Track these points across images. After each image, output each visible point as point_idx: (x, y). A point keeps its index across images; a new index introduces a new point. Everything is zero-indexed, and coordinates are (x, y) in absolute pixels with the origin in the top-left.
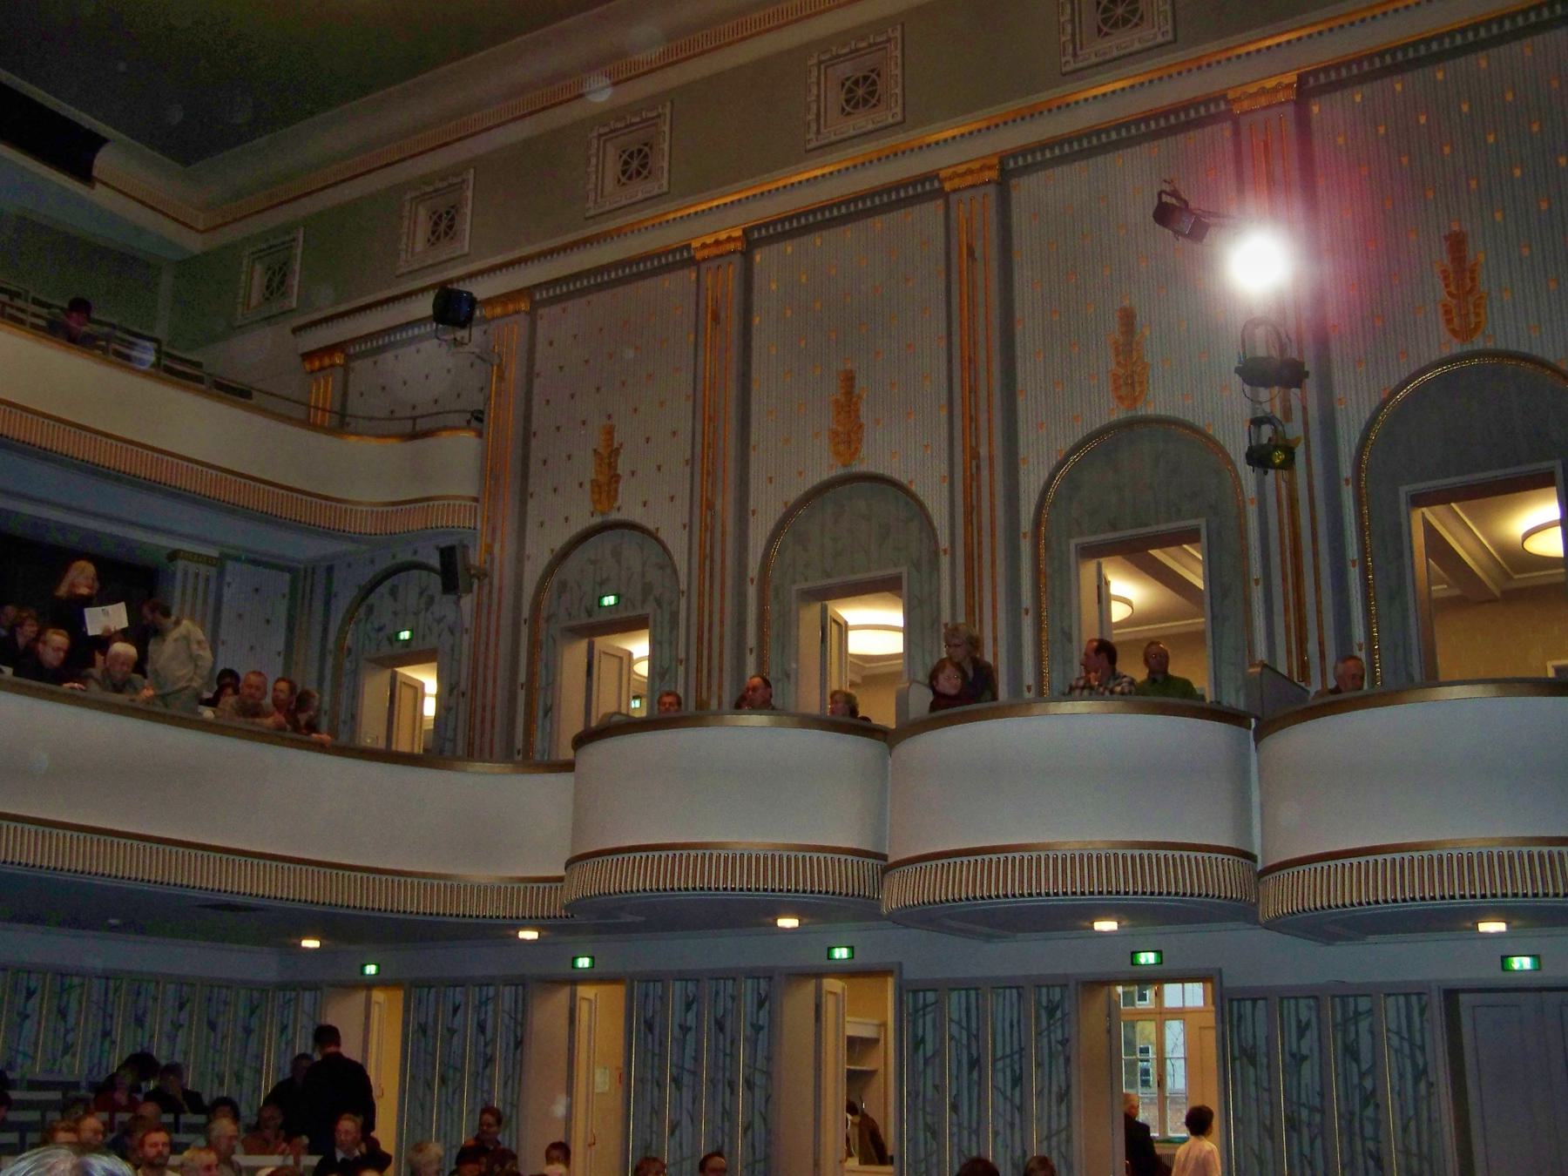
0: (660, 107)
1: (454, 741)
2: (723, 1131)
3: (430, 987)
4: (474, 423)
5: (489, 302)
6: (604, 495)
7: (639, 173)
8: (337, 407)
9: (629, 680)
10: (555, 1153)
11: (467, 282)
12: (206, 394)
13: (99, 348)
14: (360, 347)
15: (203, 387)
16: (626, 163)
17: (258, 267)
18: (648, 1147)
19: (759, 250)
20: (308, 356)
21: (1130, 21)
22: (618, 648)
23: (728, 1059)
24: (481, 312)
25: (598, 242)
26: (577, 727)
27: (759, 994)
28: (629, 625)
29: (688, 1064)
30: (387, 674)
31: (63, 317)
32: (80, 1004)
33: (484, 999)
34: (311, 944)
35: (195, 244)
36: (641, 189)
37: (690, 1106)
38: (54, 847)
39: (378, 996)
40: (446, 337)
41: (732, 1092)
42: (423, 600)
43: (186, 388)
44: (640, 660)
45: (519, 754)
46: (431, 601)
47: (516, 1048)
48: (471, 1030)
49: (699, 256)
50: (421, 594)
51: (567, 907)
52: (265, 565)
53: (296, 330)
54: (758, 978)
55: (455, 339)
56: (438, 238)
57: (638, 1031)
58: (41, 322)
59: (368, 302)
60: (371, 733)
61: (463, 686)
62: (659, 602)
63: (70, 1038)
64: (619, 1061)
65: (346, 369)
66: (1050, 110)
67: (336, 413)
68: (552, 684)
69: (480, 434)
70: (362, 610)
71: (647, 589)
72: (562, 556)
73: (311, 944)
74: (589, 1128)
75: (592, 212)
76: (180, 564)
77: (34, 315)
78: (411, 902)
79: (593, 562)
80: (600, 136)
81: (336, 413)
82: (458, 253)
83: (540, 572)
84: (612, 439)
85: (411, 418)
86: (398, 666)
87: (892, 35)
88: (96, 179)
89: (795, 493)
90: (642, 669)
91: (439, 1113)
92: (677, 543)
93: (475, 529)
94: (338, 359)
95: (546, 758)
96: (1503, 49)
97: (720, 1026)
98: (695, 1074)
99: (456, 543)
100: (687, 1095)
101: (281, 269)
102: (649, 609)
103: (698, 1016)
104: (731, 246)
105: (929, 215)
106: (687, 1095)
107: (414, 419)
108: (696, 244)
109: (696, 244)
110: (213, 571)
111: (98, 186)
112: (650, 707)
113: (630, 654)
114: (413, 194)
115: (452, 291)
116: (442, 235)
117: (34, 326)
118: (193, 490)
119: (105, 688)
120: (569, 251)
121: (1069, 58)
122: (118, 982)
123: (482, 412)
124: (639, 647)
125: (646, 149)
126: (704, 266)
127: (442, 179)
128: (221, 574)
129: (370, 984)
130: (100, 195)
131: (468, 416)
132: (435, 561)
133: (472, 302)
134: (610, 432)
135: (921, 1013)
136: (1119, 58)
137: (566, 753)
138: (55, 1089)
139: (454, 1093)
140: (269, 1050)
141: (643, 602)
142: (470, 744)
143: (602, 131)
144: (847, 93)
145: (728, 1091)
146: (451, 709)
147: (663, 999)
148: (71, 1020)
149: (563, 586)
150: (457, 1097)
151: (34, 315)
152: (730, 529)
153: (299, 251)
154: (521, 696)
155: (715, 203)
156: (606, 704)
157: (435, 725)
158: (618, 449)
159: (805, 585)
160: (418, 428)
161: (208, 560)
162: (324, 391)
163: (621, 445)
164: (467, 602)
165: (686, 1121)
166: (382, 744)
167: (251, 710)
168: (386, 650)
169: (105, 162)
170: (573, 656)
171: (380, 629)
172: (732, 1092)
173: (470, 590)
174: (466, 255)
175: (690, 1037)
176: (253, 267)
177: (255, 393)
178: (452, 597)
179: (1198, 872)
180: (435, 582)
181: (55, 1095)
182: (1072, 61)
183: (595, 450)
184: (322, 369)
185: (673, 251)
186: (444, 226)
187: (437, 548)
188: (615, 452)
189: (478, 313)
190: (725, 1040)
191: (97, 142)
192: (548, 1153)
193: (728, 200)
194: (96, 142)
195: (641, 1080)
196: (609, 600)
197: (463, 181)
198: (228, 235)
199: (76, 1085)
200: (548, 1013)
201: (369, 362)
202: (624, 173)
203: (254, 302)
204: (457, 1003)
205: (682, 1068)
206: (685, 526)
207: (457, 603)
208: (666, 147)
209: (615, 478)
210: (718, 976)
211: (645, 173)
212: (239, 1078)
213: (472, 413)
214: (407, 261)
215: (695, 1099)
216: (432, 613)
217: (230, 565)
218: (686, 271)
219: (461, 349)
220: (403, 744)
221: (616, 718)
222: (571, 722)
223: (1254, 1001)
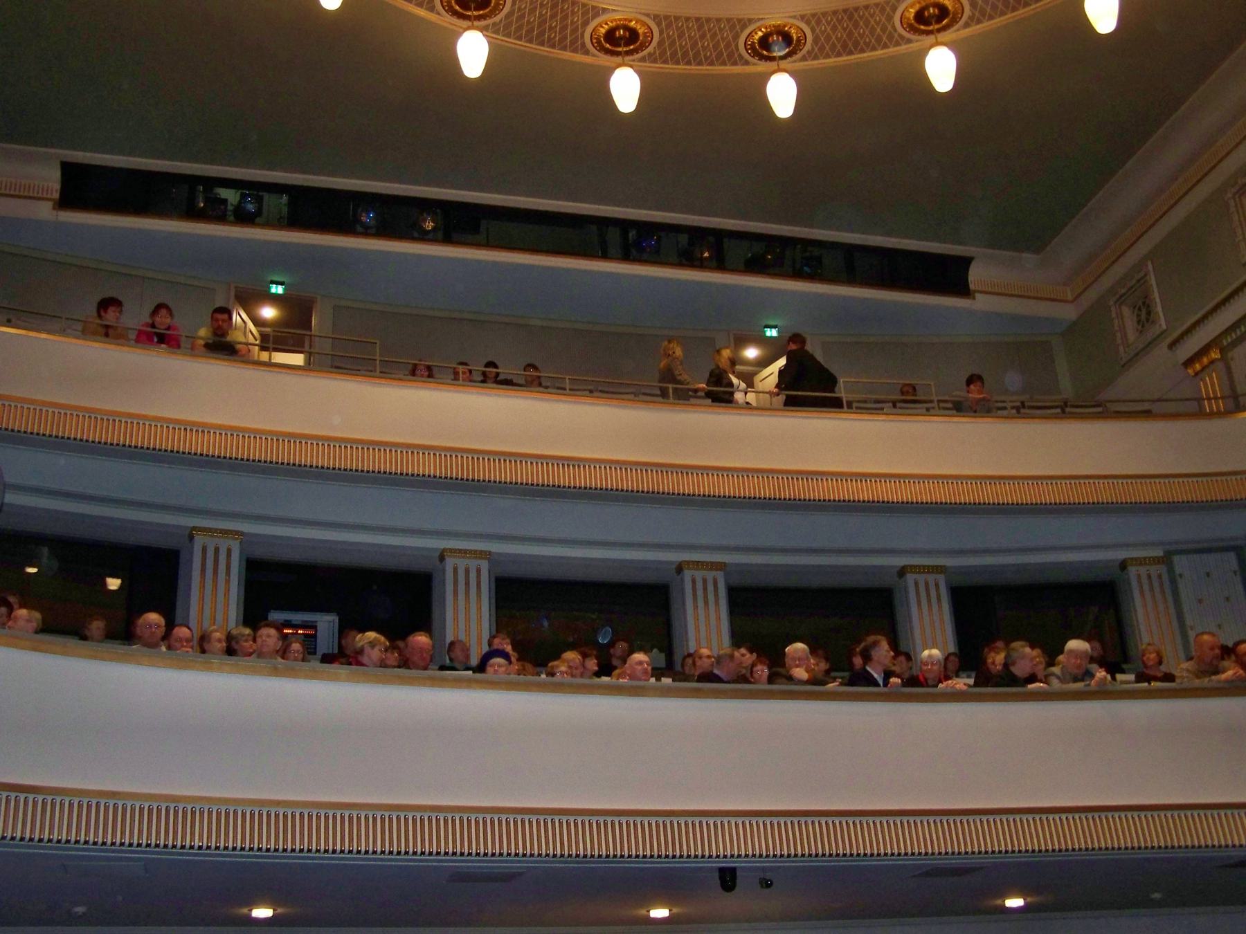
17: (1126, 311)
20: (1189, 362)
35: (1069, 313)
38: (1080, 828)
52: (1209, 550)
53: (1172, 346)
67: (1229, 397)
76: (910, 578)
88: (975, 291)
94: (1215, 355)
101: (1144, 303)
111: (977, 295)
114: (1234, 190)
118: (1181, 500)
128: (1171, 570)
130: (981, 303)
153: (1153, 282)
162: (1212, 384)
169: (975, 275)
179: (978, 839)
184: (1203, 369)
191: (965, 262)
194: (964, 263)
198: (1092, 294)
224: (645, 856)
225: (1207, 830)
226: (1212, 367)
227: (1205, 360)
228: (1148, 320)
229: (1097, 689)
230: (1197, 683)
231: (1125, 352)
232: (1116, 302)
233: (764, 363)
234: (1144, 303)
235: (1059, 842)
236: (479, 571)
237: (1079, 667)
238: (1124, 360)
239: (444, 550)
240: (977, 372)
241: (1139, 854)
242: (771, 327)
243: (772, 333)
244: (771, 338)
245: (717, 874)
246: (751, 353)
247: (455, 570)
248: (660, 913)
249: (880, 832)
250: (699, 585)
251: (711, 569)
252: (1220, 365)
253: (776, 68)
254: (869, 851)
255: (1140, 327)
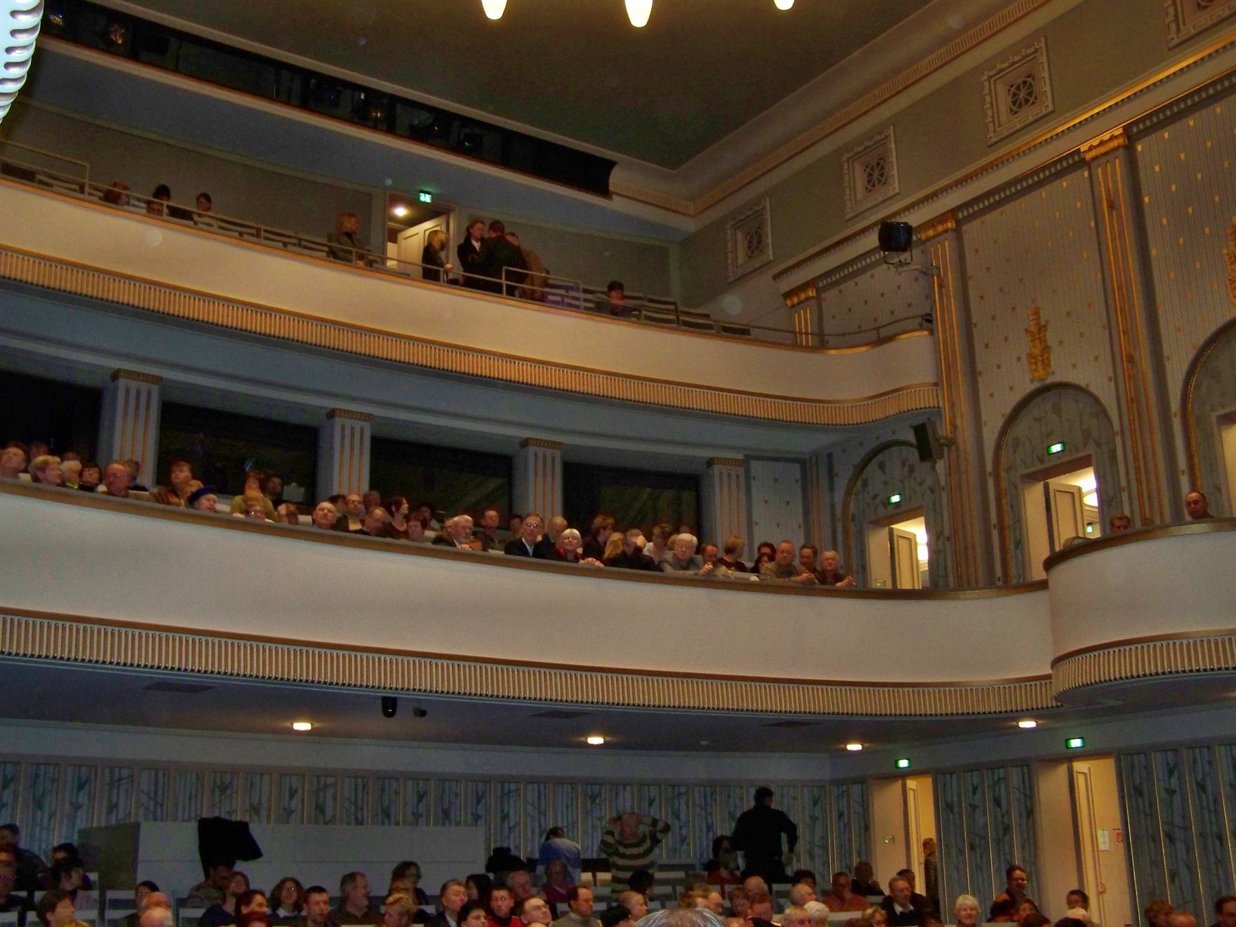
0: (1036, 43)
1: (946, 577)
2: (1219, 879)
3: (951, 774)
4: (925, 324)
5: (924, 227)
6: (1040, 364)
7: (1027, 101)
8: (816, 331)
9: (1082, 512)
10: (1074, 897)
11: (902, 215)
12: (717, 336)
13: (634, 316)
14: (875, 257)
15: (713, 331)
16: (1015, 95)
17: (740, 235)
18: (1152, 894)
19: (1140, 142)
20: (788, 295)
21: (1029, 100)
22: (1062, 485)
23: (1213, 815)
24: (917, 236)
25: (987, 171)
26: (1045, 553)
27: (1168, 763)
28: (1074, 465)
29: (1178, 821)
30: (885, 531)
31: (605, 297)
32: (688, 807)
33: (321, 786)
34: (854, 747)
35: (690, 226)
36: (1029, 114)
37: (1185, 858)
38: (611, 689)
39: (911, 783)
40: (893, 261)
41: (1222, 843)
42: (906, 469)
43: (702, 335)
44: (1089, 493)
45: (999, 580)
46: (912, 470)
47: (1028, 818)
48: (989, 805)
49: (1088, 156)
50: (903, 465)
51: (1056, 699)
53: (775, 277)
54: (1166, 751)
55: (900, 261)
56: (874, 186)
57: (1130, 796)
58: (591, 305)
59: (826, 245)
60: (879, 578)
61: (947, 533)
62: (1098, 444)
63: (684, 832)
64: (1118, 824)
65: (818, 298)
66: (1013, 157)
67: (816, 335)
68: (1019, 521)
69: (932, 332)
70: (859, 484)
71: (1087, 434)
72: (1012, 419)
73: (854, 747)
74: (1099, 880)
75: (994, 140)
77: (585, 300)
78: (929, 706)
79: (1038, 420)
80: (990, 77)
81: (816, 335)
82: (891, 194)
83: (996, 435)
84: (1039, 319)
85: (874, 329)
86: (894, 524)
87: (1037, 47)
89: (1201, 337)
90: (1092, 500)
91: (972, 877)
92: (1104, 391)
93: (939, 407)
95: (1022, 580)
96: (1204, 112)
97: (1202, 787)
98: (1186, 828)
99: (925, 421)
100: (1180, 846)
102: (1091, 450)
103: (1181, 779)
104: (1115, 143)
105: (1076, 181)
106: (1180, 846)
107: (878, 329)
108: (1084, 148)
109: (1084, 148)
110: (741, 471)
111: (614, 197)
112: (1103, 530)
113: (1079, 489)
115: (891, 224)
116: (876, 182)
117: (586, 308)
119: (675, 569)
120: (930, 200)
121: (992, 135)
122: (713, 790)
123: (930, 315)
124: (1087, 482)
125: (1030, 80)
126: (1094, 164)
127: (1028, 47)
128: (748, 471)
129: (904, 775)
130: (617, 204)
131: (920, 320)
132: (911, 437)
133: (909, 229)
134: (1037, 312)
135: (116, 784)
136: (997, 142)
137: (1038, 574)
138: (679, 870)
139: (981, 857)
140: (832, 833)
141: (1085, 445)
142: (959, 578)
143: (992, 73)
144: (1013, 98)
145: (1217, 843)
146: (940, 551)
147: (1147, 767)
148: (683, 817)
149: (1017, 443)
150: (984, 861)
151: (585, 300)
152: (1150, 377)
154: (995, 534)
155: (1096, 111)
156: (1065, 533)
157: (929, 566)
158: (1045, 326)
159: (1222, 412)
160: (881, 336)
161: (736, 462)
162: (804, 319)
163: (1047, 322)
164: (940, 466)
165: (1183, 871)
166: (889, 586)
167: (787, 570)
168: (882, 512)
169: (616, 179)
170: (1033, 497)
171: (874, 498)
172: (1222, 843)
173: (942, 457)
174: (898, 194)
175: (1177, 799)
176: (735, 235)
177: (752, 330)
178: (928, 464)
180: (914, 455)
181: (680, 874)
182: (1176, 38)
183: (1026, 330)
184: (800, 303)
185: (1066, 158)
186: (877, 175)
187: (911, 426)
188: (1042, 328)
189: (914, 238)
190: (1144, 802)
191: (609, 165)
192: (1068, 897)
193: (1113, 102)
195: (1136, 838)
196: (1056, 448)
197: (886, 137)
199: (692, 867)
200: (1051, 785)
201: (851, 283)
202: (1014, 103)
203: (740, 262)
204: (294, 787)
205: (1174, 826)
206: (1110, 379)
207: (933, 468)
208: (1046, 74)
209: (1046, 349)
210: (1192, 746)
211: (1032, 100)
212: (812, 856)
213: (922, 316)
214: (852, 209)
215: (1189, 849)
216: (915, 478)
217: (755, 465)
218: (1079, 172)
219: (905, 269)
220: (905, 584)
221: (1077, 542)
222: (1039, 550)
223: (262, 775)
224: (319, 682)
225: (543, 685)
226: (808, 303)
227: (803, 296)
228: (757, 248)
229: (703, 578)
230: (780, 581)
231: (734, 272)
232: (732, 226)
233: (411, 222)
234: (756, 232)
235: (460, 686)
236: (149, 393)
237: (687, 557)
238: (732, 279)
239: (119, 371)
240: (619, 280)
241: (413, 695)
242: (425, 192)
243: (425, 198)
244: (424, 203)
245: (380, 701)
246: (401, 212)
247: (128, 391)
248: (302, 726)
249: (130, 643)
250: (348, 432)
251: (360, 419)
252: (813, 302)
253: (881, 330)
254: (657, 704)
255: (749, 253)
